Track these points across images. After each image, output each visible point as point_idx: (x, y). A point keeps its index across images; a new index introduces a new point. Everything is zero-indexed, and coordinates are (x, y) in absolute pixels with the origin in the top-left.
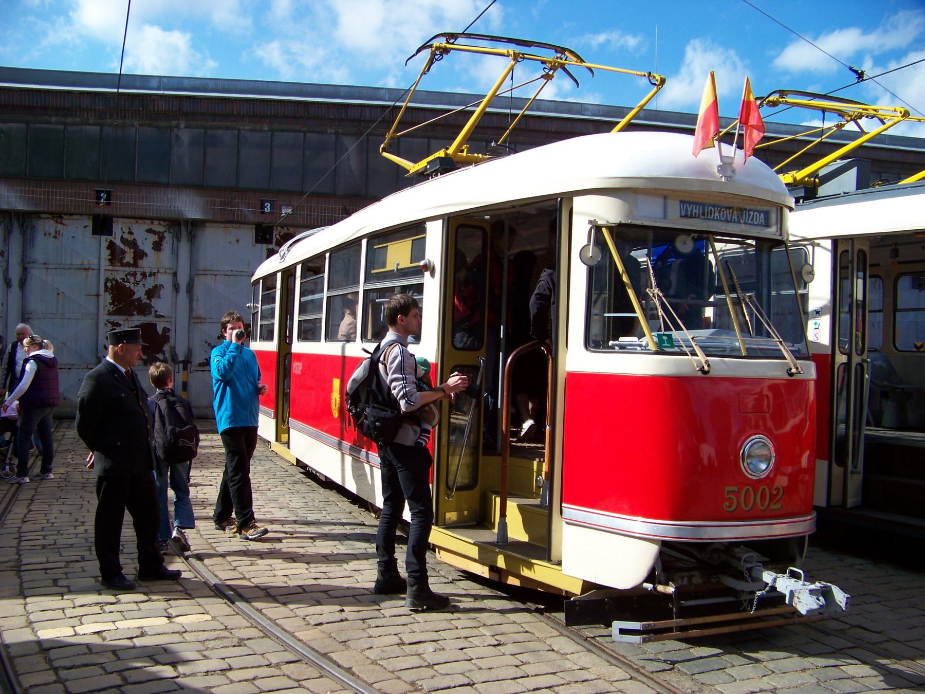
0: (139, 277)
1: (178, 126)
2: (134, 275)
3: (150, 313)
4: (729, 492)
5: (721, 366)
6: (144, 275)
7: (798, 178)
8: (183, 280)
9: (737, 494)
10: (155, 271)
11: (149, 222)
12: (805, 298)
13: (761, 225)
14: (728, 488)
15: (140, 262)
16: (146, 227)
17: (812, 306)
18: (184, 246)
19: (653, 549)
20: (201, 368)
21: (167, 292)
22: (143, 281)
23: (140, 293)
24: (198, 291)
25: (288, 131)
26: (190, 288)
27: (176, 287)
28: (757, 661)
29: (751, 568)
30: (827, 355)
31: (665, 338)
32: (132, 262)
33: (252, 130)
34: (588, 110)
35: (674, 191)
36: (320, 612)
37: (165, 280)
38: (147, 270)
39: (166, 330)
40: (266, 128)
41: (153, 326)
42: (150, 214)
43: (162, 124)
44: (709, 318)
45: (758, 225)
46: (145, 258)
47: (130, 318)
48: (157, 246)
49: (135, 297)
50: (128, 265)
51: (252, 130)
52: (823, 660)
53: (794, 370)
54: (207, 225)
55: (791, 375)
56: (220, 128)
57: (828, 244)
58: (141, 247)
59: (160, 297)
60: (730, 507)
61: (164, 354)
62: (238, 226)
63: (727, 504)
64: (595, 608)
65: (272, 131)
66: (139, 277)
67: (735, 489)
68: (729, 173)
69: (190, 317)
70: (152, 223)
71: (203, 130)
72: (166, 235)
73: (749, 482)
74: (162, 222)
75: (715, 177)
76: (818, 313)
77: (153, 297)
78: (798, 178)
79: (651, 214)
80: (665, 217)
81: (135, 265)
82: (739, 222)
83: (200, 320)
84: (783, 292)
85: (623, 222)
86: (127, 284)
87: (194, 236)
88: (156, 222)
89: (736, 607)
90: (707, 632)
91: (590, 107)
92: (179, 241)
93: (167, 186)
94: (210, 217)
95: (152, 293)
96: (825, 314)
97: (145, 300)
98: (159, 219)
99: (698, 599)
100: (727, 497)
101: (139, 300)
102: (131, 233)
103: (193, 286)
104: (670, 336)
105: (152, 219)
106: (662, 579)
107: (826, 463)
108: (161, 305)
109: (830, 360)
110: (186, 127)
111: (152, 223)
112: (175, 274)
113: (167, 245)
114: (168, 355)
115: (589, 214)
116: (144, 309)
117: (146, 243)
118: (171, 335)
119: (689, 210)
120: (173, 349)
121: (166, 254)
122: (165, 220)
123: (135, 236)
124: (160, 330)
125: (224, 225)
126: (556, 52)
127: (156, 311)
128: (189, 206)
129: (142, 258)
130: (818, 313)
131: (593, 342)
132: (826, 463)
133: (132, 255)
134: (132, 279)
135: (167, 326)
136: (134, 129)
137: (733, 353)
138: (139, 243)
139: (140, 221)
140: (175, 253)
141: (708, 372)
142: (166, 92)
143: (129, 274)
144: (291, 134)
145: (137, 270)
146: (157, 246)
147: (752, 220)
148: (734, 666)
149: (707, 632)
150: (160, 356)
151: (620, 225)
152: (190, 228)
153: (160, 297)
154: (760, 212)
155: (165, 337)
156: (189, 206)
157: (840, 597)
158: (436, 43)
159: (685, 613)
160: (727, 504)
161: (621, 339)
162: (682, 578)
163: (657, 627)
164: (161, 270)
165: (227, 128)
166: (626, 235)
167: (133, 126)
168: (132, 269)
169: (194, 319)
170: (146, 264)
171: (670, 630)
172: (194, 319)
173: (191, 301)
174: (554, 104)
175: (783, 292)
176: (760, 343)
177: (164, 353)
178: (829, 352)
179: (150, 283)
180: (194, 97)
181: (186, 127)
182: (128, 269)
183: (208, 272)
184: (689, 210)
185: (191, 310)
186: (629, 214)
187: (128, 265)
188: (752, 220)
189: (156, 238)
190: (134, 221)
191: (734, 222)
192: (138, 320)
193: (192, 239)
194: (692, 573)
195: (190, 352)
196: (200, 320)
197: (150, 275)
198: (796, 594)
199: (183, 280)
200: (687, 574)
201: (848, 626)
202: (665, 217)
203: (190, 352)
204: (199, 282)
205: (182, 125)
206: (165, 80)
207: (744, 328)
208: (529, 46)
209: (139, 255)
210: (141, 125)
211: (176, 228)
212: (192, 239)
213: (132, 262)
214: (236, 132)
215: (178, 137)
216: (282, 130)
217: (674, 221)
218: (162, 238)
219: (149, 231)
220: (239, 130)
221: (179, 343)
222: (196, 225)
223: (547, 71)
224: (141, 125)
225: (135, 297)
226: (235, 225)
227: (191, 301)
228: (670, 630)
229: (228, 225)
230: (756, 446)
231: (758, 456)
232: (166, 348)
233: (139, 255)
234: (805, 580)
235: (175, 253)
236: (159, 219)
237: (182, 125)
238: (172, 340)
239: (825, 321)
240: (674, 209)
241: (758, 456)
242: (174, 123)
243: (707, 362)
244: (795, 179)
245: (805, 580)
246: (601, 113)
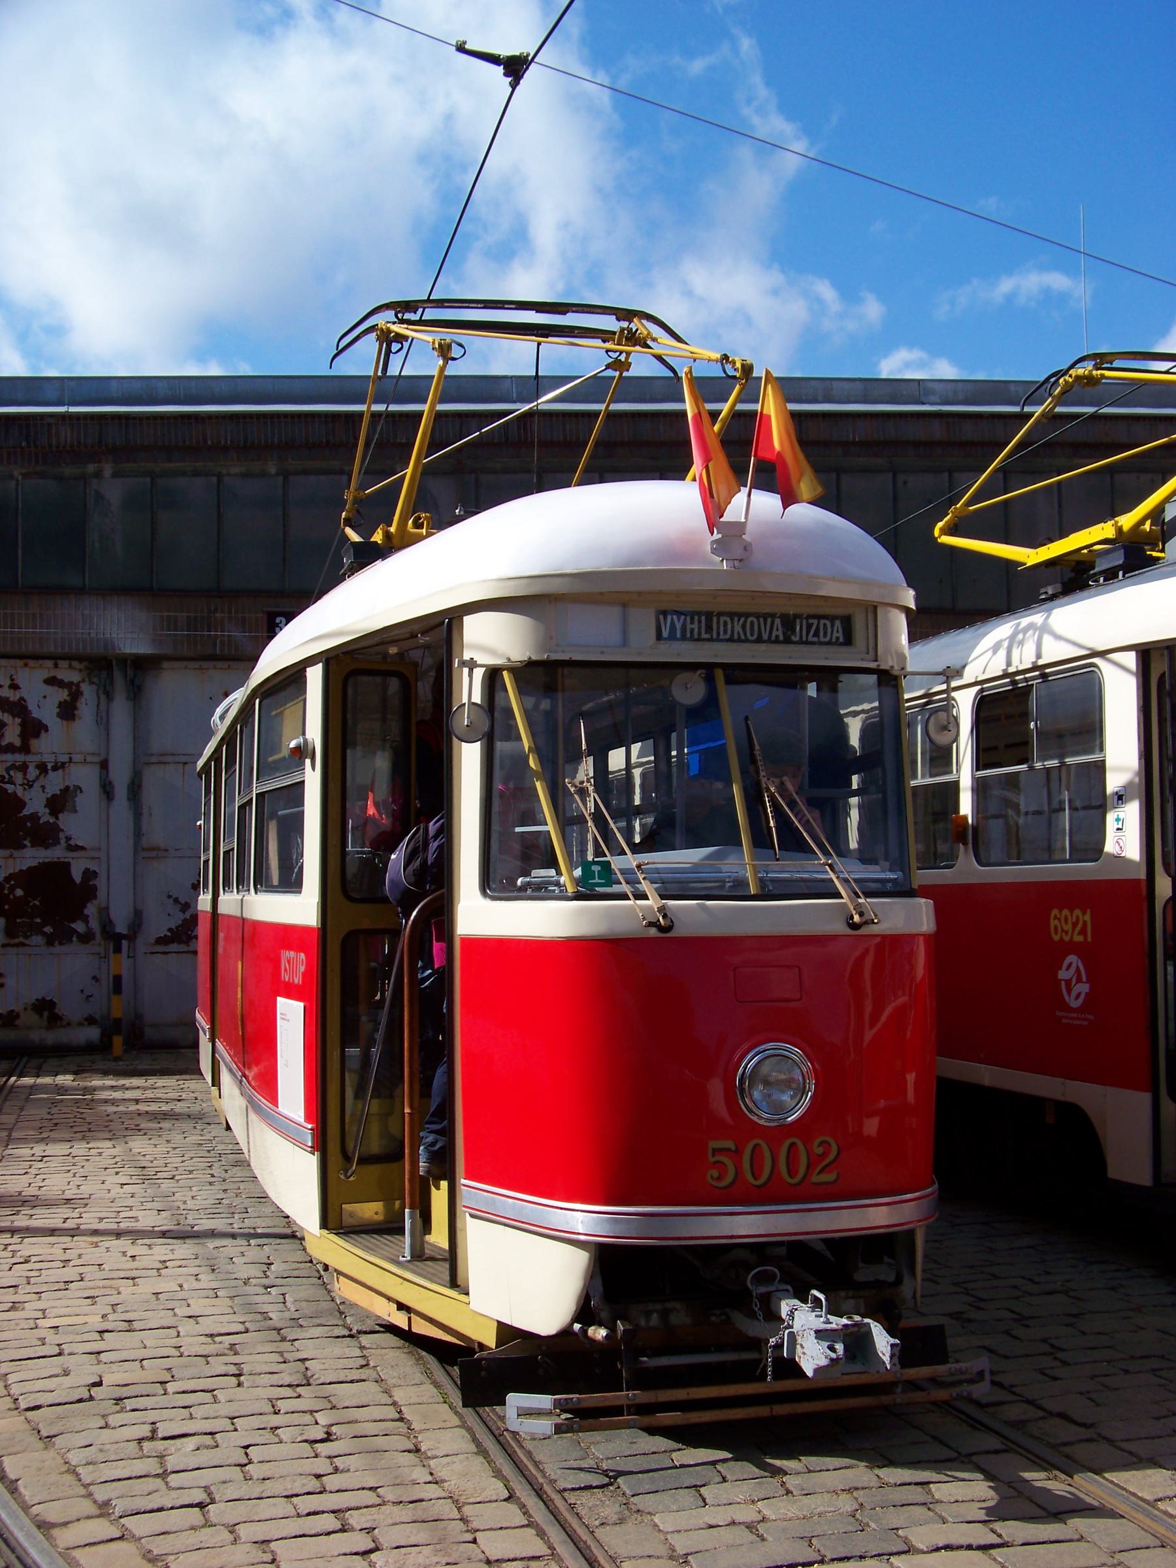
0: (32, 772)
1: (98, 475)
2: (24, 768)
3: (57, 842)
4: (716, 1151)
5: (693, 915)
6: (43, 768)
7: (1126, 528)
8: (120, 776)
9: (737, 1153)
10: (65, 758)
11: (50, 663)
12: (1100, 767)
13: (837, 643)
14: (713, 1144)
15: (34, 744)
16: (45, 674)
17: (1114, 782)
18: (120, 710)
19: (579, 1260)
20: (162, 948)
21: (89, 800)
22: (42, 781)
23: (35, 803)
24: (152, 795)
25: (318, 472)
26: (135, 789)
27: (107, 790)
28: (781, 1472)
29: (769, 1294)
30: (1138, 881)
31: (596, 868)
32: (18, 742)
33: (245, 475)
34: (933, 392)
35: (640, 593)
36: (171, 1417)
37: (85, 777)
38: (49, 759)
39: (89, 875)
40: (273, 470)
41: (63, 868)
42: (51, 649)
43: (68, 471)
44: (965, 817)
45: (829, 643)
46: (43, 734)
47: (16, 853)
48: (67, 711)
49: (26, 812)
50: (10, 749)
51: (245, 475)
52: (934, 1474)
53: (856, 918)
54: (165, 665)
55: (854, 926)
56: (184, 474)
57: (1130, 659)
58: (36, 714)
59: (76, 811)
60: (719, 1179)
61: (87, 922)
62: (226, 664)
63: (715, 1173)
64: (486, 1372)
65: (285, 474)
66: (32, 772)
67: (730, 1144)
68: (738, 553)
69: (138, 848)
70: (56, 666)
71: (148, 480)
72: (86, 688)
73: (757, 1130)
74: (75, 664)
75: (713, 563)
76: (1120, 798)
77: (61, 811)
78: (1126, 528)
79: (594, 637)
80: (625, 643)
81: (25, 749)
82: (787, 641)
83: (158, 852)
84: (1069, 760)
85: (534, 658)
86: (10, 788)
87: (139, 688)
88: (63, 664)
89: (751, 1371)
90: (696, 1417)
91: (936, 386)
92: (110, 697)
93: (81, 591)
94: (168, 650)
95: (60, 803)
96: (1131, 799)
97: (46, 817)
98: (69, 658)
99: (660, 1355)
100: (712, 1160)
101: (34, 817)
102: (14, 687)
103: (140, 786)
104: (606, 866)
105: (56, 658)
106: (604, 1315)
107: (1146, 1098)
108: (79, 825)
109: (1144, 891)
110: (116, 475)
111: (56, 666)
112: (104, 765)
113: (86, 708)
114: (94, 924)
115: (491, 641)
116: (46, 835)
117: (45, 705)
118: (101, 883)
119: (678, 626)
120: (104, 911)
121: (84, 730)
122: (80, 659)
123: (23, 693)
124: (77, 876)
125: (197, 664)
126: (618, 319)
127: (68, 839)
128: (126, 630)
129: (37, 736)
130: (1120, 798)
131: (493, 883)
132: (1146, 1098)
133: (18, 730)
134: (18, 777)
135: (93, 866)
136: (13, 484)
137: (737, 891)
138: (32, 706)
139: (32, 663)
140: (103, 722)
141: (669, 928)
142: (73, 409)
143: (13, 767)
144: (322, 478)
145: (29, 758)
146: (67, 711)
147: (816, 634)
148: (724, 1480)
149: (696, 1417)
150: (79, 927)
151: (530, 664)
152: (130, 672)
153: (76, 811)
154: (832, 619)
155: (88, 889)
156: (126, 630)
157: (883, 1342)
158: (381, 320)
159: (645, 1379)
160: (715, 1173)
161: (535, 873)
162: (648, 1314)
163: (584, 1405)
164: (76, 758)
165: (196, 474)
166: (537, 675)
167: (11, 477)
168: (19, 758)
169: (145, 852)
170: (47, 747)
171: (617, 1410)
172: (145, 852)
173: (138, 815)
174: (858, 385)
175: (1069, 760)
176: (788, 868)
177: (86, 920)
178: (1142, 875)
179: (55, 783)
180: (127, 417)
181: (116, 475)
182: (9, 757)
183: (170, 759)
184: (678, 626)
185: (138, 834)
186: (544, 645)
187: (10, 749)
188: (816, 634)
189: (64, 695)
190: (19, 663)
191: (777, 641)
192: (31, 857)
193: (136, 693)
194: (669, 1305)
195: (138, 914)
196: (158, 852)
197: (55, 769)
198: (799, 1340)
199: (120, 776)
200: (659, 1307)
201: (1041, 1413)
202: (625, 643)
203: (138, 914)
204: (153, 777)
205: (108, 470)
206: (72, 384)
207: (761, 840)
208: (564, 313)
209: (33, 729)
210: (26, 476)
211: (104, 674)
212: (136, 693)
213: (18, 742)
214: (214, 479)
215: (99, 497)
216: (306, 472)
217: (644, 646)
218: (76, 694)
219: (51, 681)
220: (220, 477)
221: (117, 899)
222: (142, 665)
223: (615, 355)
224: (26, 476)
225: (26, 812)
226: (220, 664)
227: (138, 815)
228: (617, 1410)
229: (205, 664)
230: (767, 1061)
231: (779, 1084)
232: (91, 910)
233: (33, 729)
234: (829, 1312)
235: (103, 722)
236: (69, 658)
237: (108, 470)
238: (101, 893)
239: (1131, 812)
240: (643, 627)
241: (779, 1084)
242: (91, 468)
243: (858, 907)
244: (1119, 530)
245: (829, 1312)
246: (961, 397)
